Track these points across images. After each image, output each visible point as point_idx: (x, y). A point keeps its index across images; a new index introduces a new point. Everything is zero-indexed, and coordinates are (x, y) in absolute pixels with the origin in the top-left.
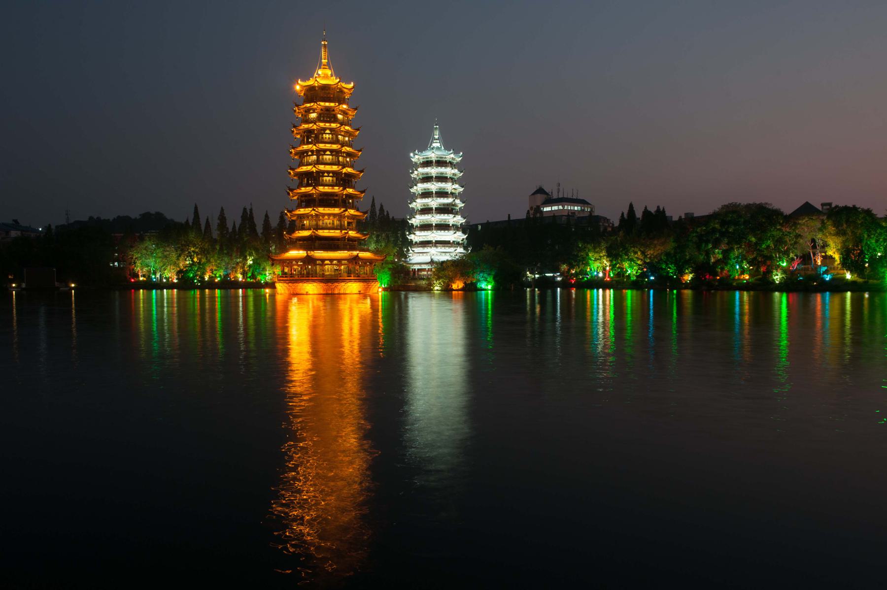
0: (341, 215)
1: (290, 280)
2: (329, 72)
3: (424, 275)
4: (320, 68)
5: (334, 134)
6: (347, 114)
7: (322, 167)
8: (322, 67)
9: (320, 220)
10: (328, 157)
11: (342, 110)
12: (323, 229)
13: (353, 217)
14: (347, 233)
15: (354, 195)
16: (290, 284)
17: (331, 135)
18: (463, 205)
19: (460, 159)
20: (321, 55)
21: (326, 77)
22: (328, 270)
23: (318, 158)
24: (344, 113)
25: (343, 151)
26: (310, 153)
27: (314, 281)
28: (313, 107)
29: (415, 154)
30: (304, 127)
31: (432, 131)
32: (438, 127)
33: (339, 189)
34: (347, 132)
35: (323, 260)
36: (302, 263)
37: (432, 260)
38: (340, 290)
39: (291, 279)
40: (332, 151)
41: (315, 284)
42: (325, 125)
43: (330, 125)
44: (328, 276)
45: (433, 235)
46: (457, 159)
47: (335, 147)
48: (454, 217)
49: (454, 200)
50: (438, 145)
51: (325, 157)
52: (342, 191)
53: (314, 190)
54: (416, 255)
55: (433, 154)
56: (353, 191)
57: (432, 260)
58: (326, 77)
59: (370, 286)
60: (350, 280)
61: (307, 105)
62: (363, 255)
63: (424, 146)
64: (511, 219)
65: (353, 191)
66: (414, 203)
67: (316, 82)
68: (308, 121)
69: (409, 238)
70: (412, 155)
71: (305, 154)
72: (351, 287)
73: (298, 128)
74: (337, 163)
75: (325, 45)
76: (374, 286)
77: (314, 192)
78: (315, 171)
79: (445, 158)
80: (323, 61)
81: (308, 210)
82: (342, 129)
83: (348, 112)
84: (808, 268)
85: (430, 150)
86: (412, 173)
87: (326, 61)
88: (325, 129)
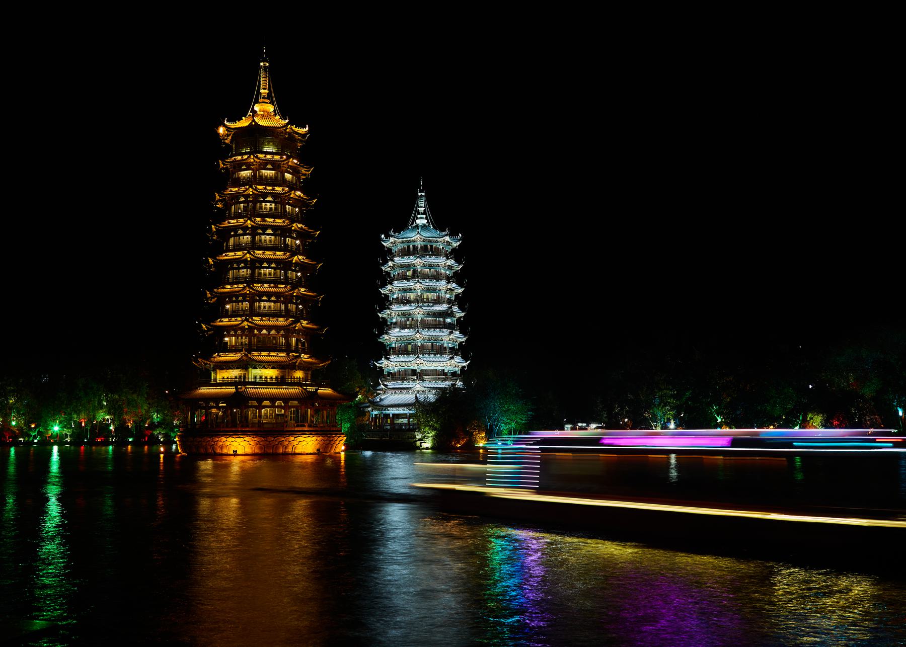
2: (270, 108)
4: (257, 102)
5: (279, 203)
7: (259, 253)
8: (261, 100)
14: (299, 356)
17: (273, 205)
18: (463, 314)
19: (458, 243)
20: (260, 81)
21: (266, 115)
22: (266, 415)
27: (245, 433)
29: (388, 236)
30: (231, 191)
31: (414, 200)
32: (423, 194)
36: (225, 405)
38: (286, 448)
43: (273, 189)
44: (266, 426)
45: (418, 361)
46: (453, 243)
49: (451, 308)
50: (425, 221)
51: (264, 171)
52: (291, 290)
56: (305, 291)
58: (266, 115)
59: (333, 442)
60: (303, 433)
63: (402, 223)
65: (305, 291)
72: (304, 443)
75: (265, 67)
79: (437, 242)
80: (262, 91)
81: (236, 320)
84: (351, 405)
86: (383, 264)
87: (267, 91)
88: (265, 195)
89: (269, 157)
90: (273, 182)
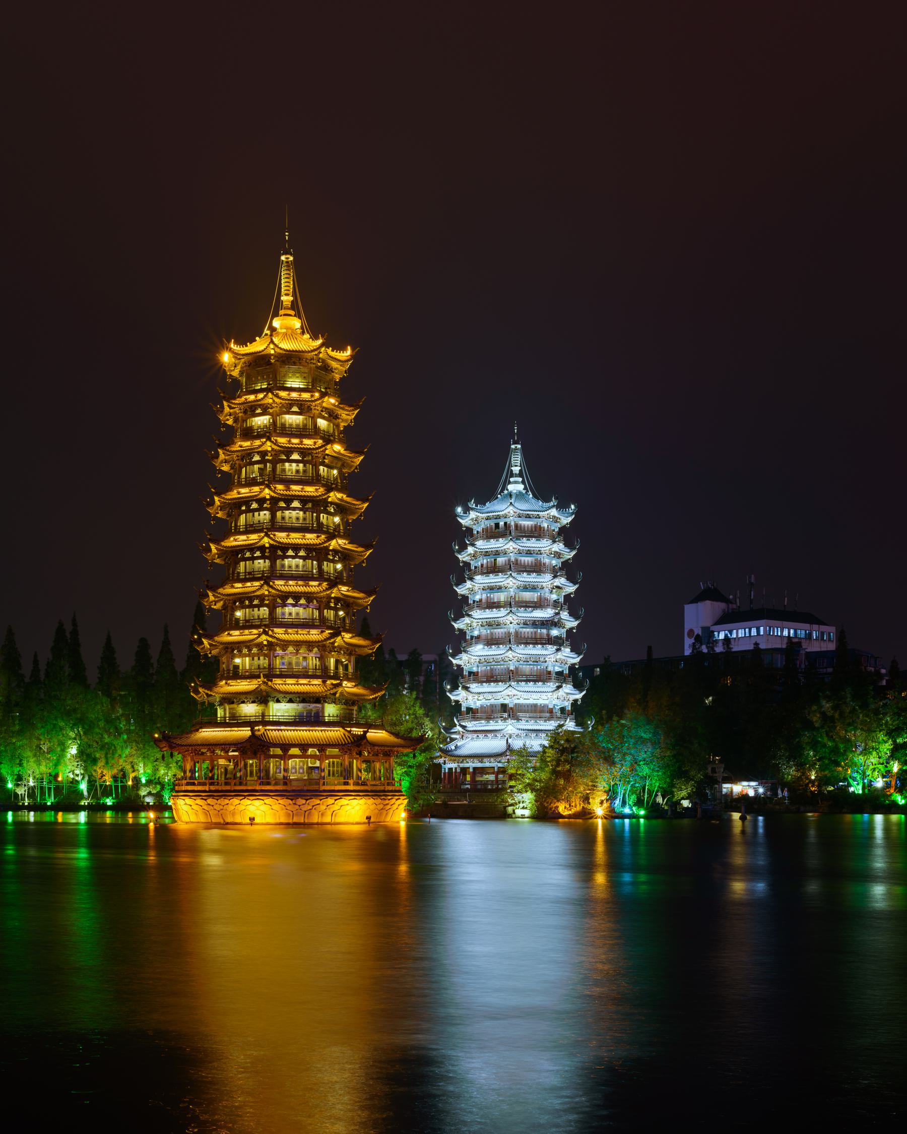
0: (324, 646)
1: (210, 791)
3: (487, 782)
4: (276, 314)
6: (337, 417)
7: (281, 536)
8: (282, 312)
9: (276, 657)
10: (294, 514)
11: (326, 409)
12: (282, 676)
13: (350, 650)
15: (352, 600)
16: (210, 801)
17: (301, 465)
19: (570, 519)
21: (290, 334)
23: (273, 516)
24: (330, 415)
25: (330, 500)
26: (254, 505)
27: (265, 793)
28: (262, 402)
29: (467, 510)
30: (241, 446)
31: (506, 454)
32: (519, 446)
33: (319, 585)
34: (337, 458)
35: (285, 746)
36: (236, 753)
37: (509, 746)
39: (212, 788)
40: (304, 500)
41: (268, 801)
42: (289, 442)
43: (301, 443)
45: (511, 691)
47: (310, 490)
48: (558, 650)
50: (521, 487)
51: (287, 417)
53: (266, 587)
54: (470, 736)
55: (511, 508)
56: (348, 591)
57: (509, 746)
58: (290, 334)
59: (388, 807)
61: (247, 397)
62: (229, 733)
64: (655, 656)
65: (348, 591)
66: (467, 620)
67: (272, 346)
68: (249, 434)
69: (453, 698)
70: (459, 510)
71: (244, 508)
73: (228, 448)
74: (319, 529)
76: (395, 806)
77: (267, 593)
78: (267, 545)
80: (284, 298)
81: (251, 634)
82: (327, 452)
83: (340, 412)
85: (502, 500)
88: (288, 451)
89: (294, 395)
90: (301, 432)
